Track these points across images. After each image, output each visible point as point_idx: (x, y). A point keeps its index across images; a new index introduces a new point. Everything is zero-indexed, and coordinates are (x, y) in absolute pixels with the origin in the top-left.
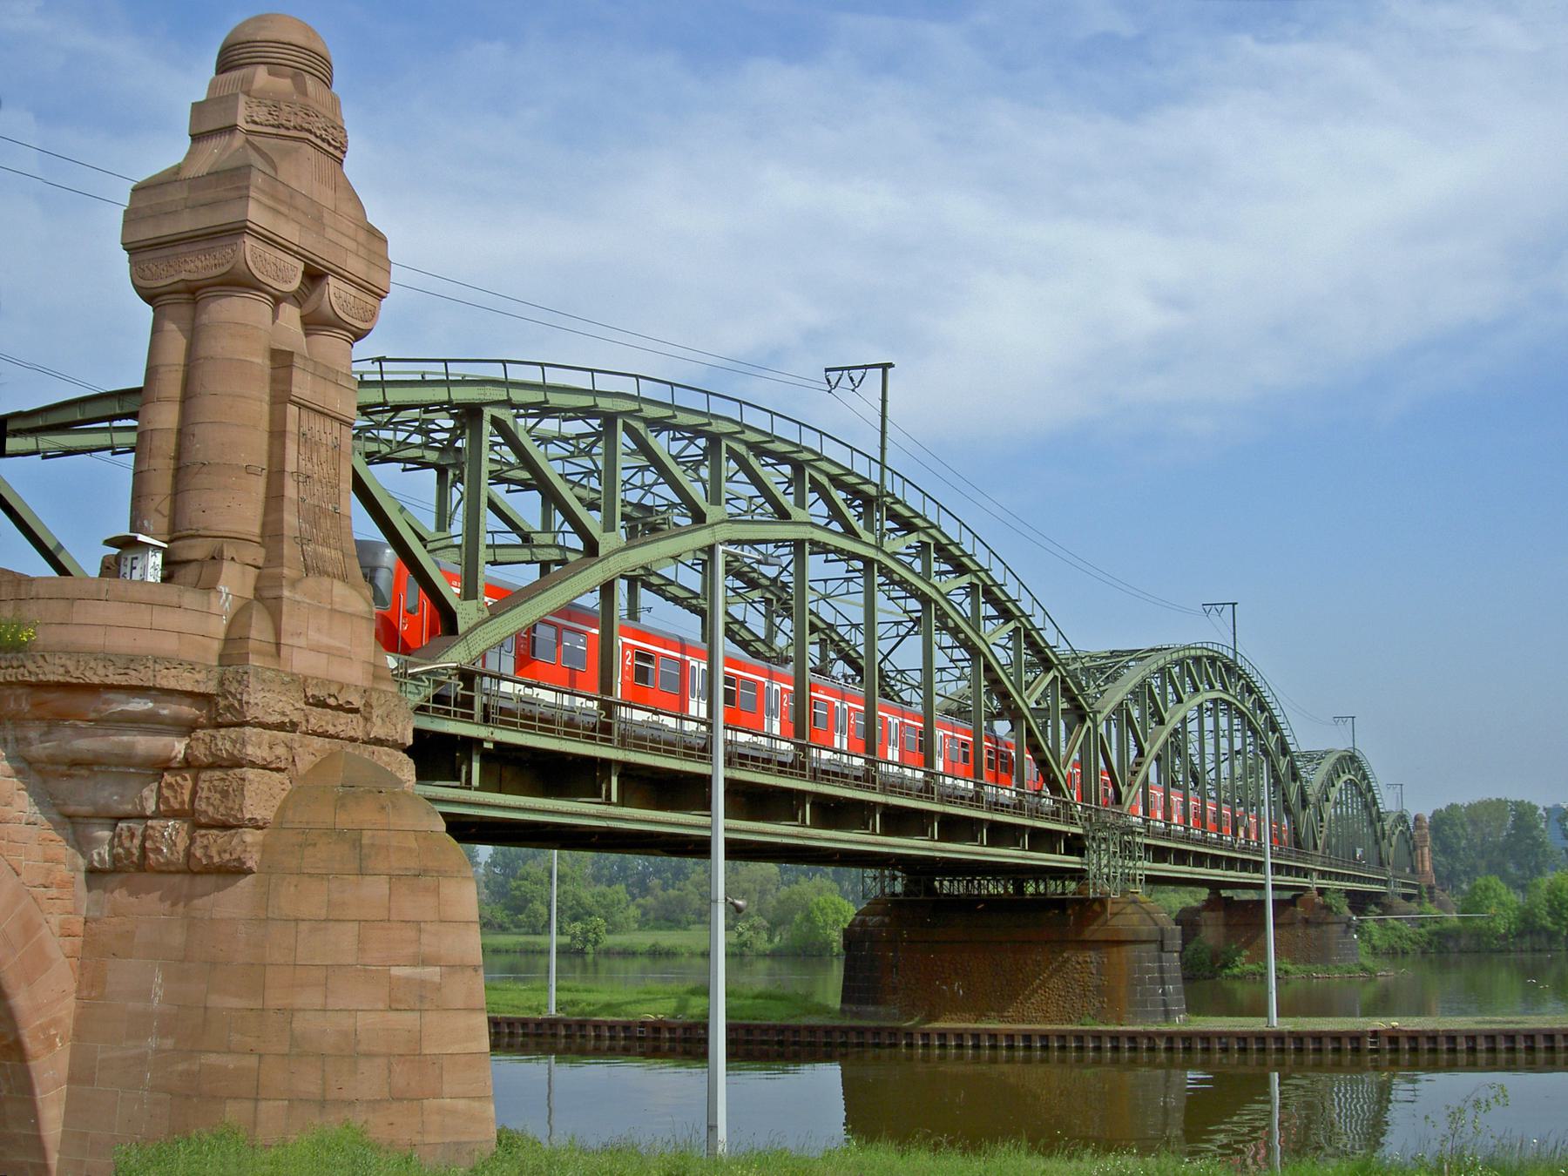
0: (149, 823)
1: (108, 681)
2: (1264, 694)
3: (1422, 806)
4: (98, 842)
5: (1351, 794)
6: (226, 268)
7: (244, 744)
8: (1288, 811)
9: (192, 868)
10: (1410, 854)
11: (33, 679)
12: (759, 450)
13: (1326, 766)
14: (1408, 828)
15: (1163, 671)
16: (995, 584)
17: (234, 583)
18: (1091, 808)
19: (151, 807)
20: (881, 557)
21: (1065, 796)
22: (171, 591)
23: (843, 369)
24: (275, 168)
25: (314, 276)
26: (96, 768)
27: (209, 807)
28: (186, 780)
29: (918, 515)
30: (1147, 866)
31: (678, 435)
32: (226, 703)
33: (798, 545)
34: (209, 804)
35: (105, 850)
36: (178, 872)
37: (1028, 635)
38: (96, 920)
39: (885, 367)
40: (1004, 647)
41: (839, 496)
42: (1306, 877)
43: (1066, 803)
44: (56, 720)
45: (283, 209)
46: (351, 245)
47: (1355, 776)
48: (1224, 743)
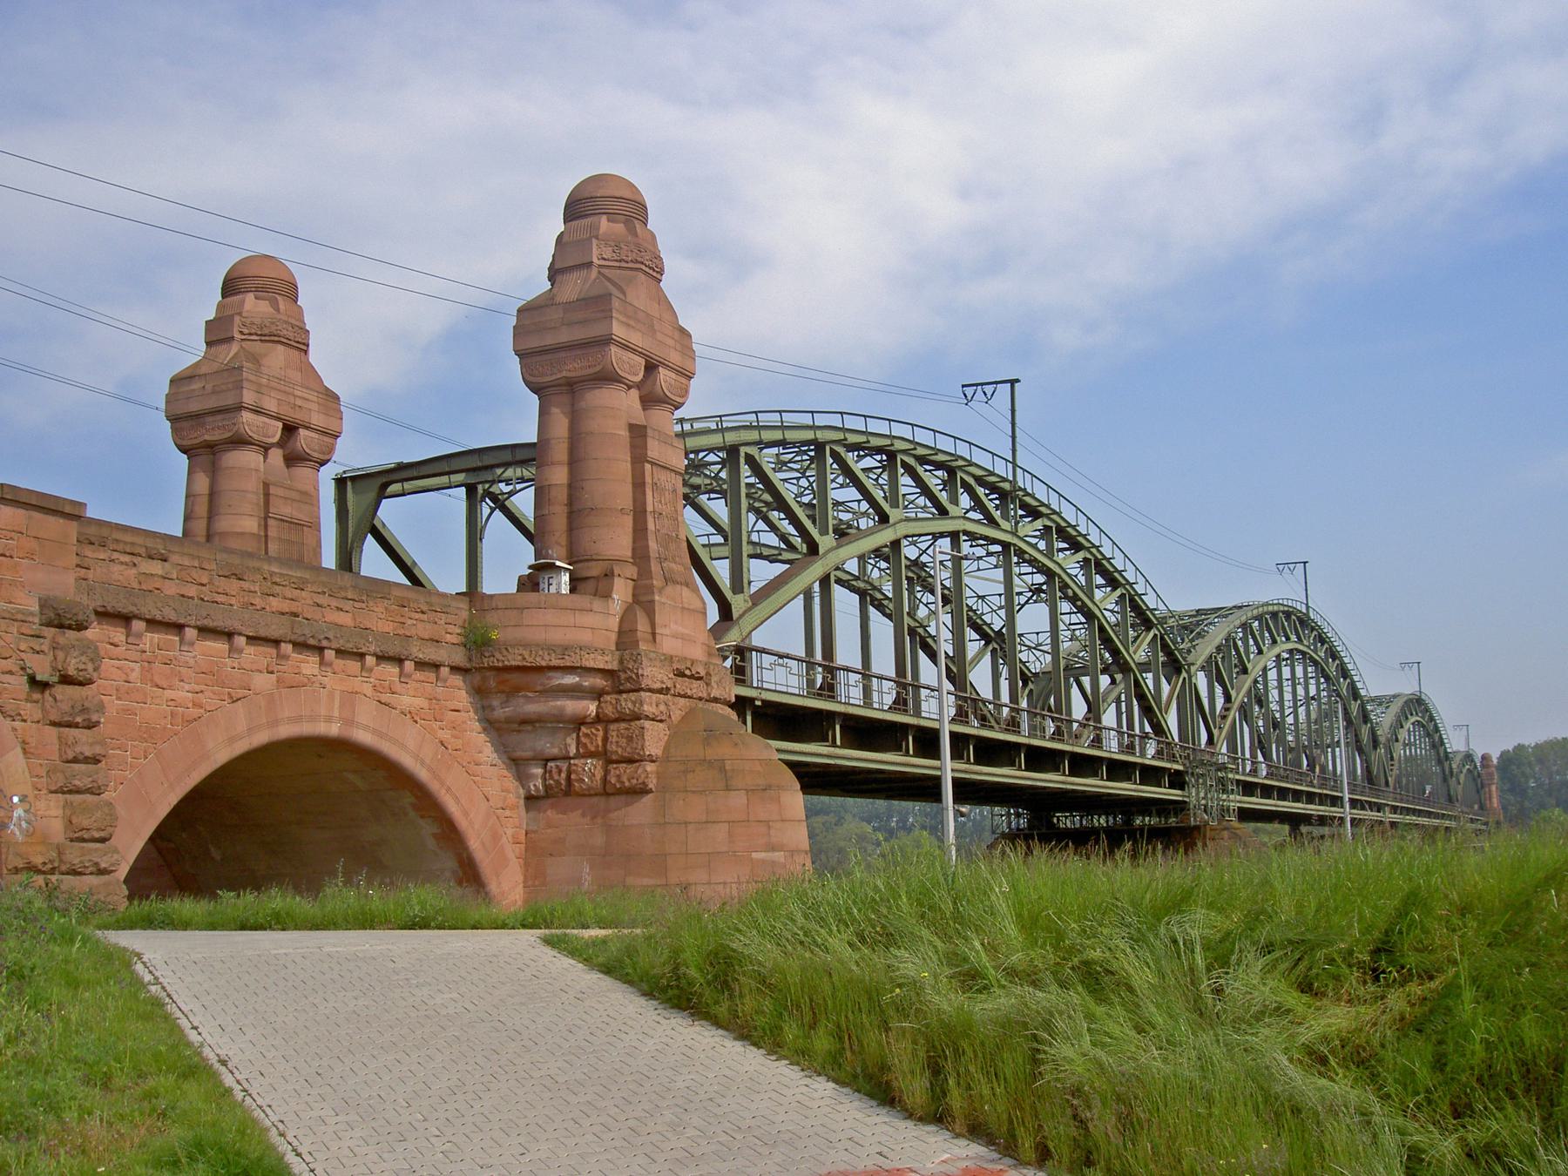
0: (572, 761)
1: (552, 664)
2: (1335, 644)
3: (1490, 744)
4: (532, 777)
5: (1420, 735)
6: (598, 369)
7: (641, 704)
8: (1360, 750)
9: (607, 791)
10: (1478, 792)
11: (500, 664)
12: (922, 460)
13: (1395, 708)
14: (1476, 767)
15: (1245, 626)
16: (1105, 558)
17: (621, 592)
18: (1189, 748)
19: (573, 751)
20: (1015, 541)
21: (1167, 738)
22: (580, 600)
23: (977, 385)
24: (624, 293)
25: (651, 368)
26: (537, 725)
27: (617, 747)
28: (598, 730)
29: (1043, 504)
30: (1237, 800)
31: (862, 453)
32: (627, 676)
33: (954, 536)
34: (618, 746)
35: (539, 783)
36: (596, 795)
37: (1132, 600)
38: (535, 832)
39: (1013, 382)
40: (1112, 611)
41: (981, 491)
42: (1379, 811)
43: (1169, 744)
44: (513, 692)
45: (632, 323)
46: (670, 342)
47: (1423, 717)
48: (1300, 691)
